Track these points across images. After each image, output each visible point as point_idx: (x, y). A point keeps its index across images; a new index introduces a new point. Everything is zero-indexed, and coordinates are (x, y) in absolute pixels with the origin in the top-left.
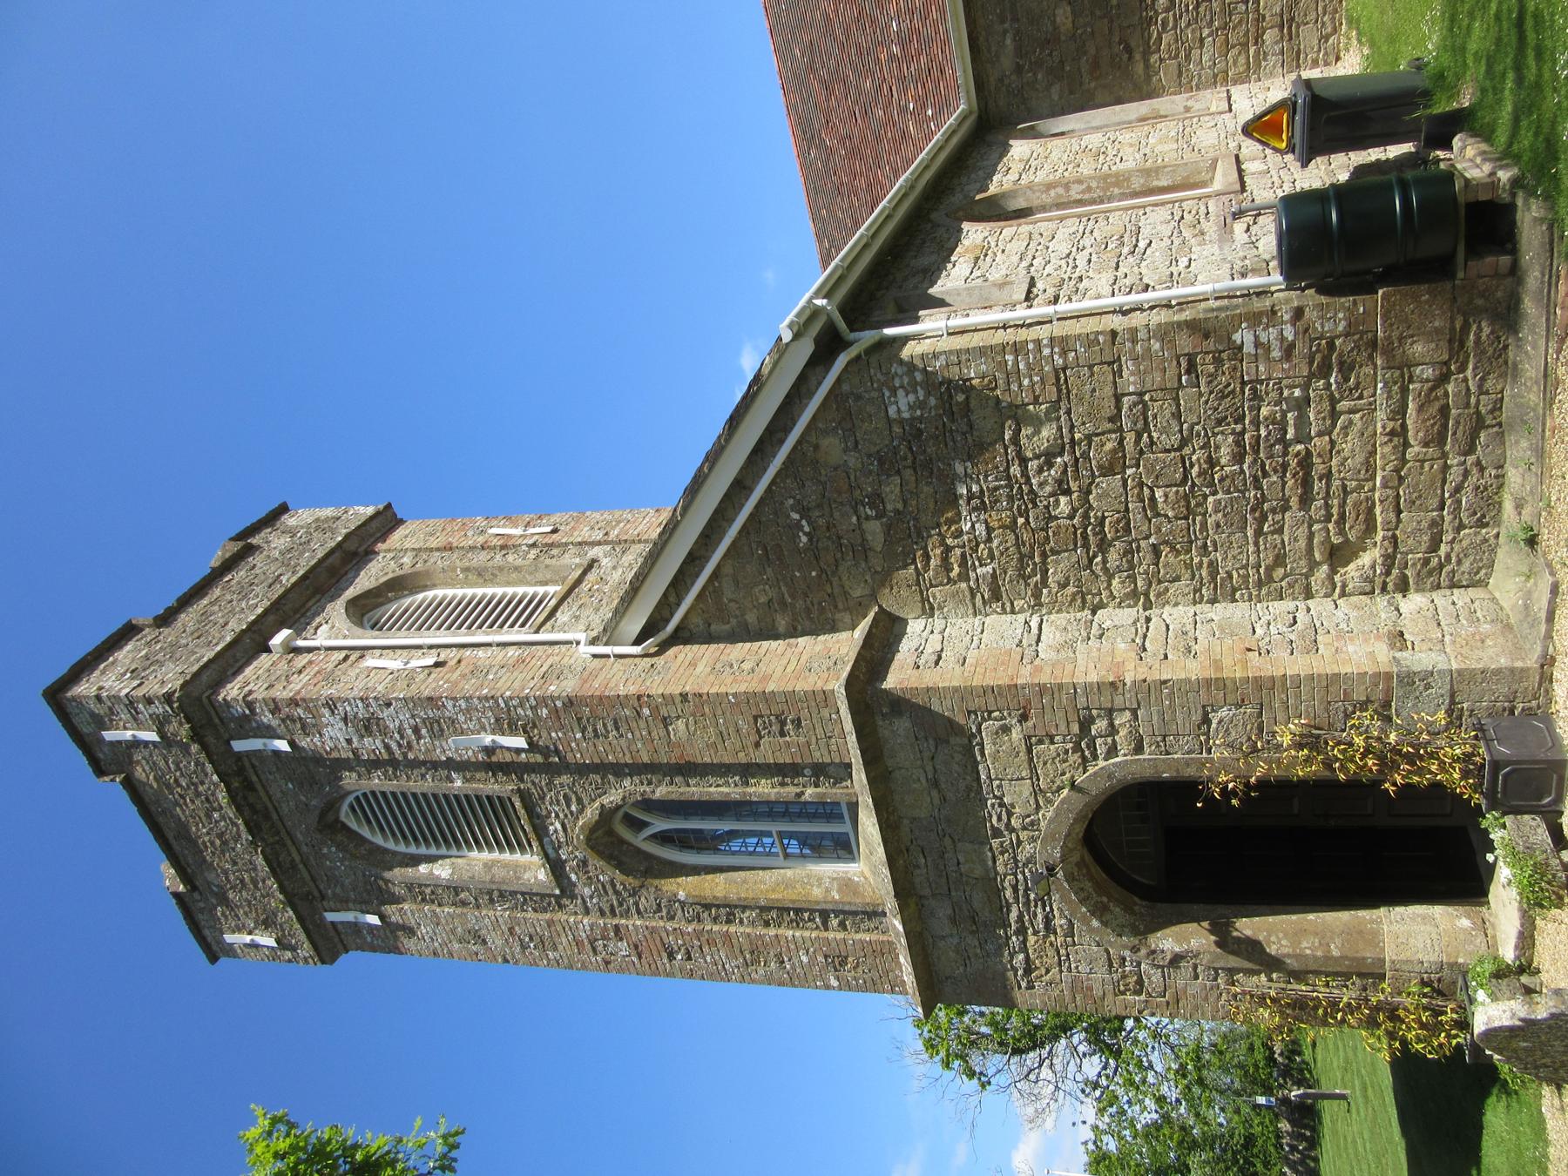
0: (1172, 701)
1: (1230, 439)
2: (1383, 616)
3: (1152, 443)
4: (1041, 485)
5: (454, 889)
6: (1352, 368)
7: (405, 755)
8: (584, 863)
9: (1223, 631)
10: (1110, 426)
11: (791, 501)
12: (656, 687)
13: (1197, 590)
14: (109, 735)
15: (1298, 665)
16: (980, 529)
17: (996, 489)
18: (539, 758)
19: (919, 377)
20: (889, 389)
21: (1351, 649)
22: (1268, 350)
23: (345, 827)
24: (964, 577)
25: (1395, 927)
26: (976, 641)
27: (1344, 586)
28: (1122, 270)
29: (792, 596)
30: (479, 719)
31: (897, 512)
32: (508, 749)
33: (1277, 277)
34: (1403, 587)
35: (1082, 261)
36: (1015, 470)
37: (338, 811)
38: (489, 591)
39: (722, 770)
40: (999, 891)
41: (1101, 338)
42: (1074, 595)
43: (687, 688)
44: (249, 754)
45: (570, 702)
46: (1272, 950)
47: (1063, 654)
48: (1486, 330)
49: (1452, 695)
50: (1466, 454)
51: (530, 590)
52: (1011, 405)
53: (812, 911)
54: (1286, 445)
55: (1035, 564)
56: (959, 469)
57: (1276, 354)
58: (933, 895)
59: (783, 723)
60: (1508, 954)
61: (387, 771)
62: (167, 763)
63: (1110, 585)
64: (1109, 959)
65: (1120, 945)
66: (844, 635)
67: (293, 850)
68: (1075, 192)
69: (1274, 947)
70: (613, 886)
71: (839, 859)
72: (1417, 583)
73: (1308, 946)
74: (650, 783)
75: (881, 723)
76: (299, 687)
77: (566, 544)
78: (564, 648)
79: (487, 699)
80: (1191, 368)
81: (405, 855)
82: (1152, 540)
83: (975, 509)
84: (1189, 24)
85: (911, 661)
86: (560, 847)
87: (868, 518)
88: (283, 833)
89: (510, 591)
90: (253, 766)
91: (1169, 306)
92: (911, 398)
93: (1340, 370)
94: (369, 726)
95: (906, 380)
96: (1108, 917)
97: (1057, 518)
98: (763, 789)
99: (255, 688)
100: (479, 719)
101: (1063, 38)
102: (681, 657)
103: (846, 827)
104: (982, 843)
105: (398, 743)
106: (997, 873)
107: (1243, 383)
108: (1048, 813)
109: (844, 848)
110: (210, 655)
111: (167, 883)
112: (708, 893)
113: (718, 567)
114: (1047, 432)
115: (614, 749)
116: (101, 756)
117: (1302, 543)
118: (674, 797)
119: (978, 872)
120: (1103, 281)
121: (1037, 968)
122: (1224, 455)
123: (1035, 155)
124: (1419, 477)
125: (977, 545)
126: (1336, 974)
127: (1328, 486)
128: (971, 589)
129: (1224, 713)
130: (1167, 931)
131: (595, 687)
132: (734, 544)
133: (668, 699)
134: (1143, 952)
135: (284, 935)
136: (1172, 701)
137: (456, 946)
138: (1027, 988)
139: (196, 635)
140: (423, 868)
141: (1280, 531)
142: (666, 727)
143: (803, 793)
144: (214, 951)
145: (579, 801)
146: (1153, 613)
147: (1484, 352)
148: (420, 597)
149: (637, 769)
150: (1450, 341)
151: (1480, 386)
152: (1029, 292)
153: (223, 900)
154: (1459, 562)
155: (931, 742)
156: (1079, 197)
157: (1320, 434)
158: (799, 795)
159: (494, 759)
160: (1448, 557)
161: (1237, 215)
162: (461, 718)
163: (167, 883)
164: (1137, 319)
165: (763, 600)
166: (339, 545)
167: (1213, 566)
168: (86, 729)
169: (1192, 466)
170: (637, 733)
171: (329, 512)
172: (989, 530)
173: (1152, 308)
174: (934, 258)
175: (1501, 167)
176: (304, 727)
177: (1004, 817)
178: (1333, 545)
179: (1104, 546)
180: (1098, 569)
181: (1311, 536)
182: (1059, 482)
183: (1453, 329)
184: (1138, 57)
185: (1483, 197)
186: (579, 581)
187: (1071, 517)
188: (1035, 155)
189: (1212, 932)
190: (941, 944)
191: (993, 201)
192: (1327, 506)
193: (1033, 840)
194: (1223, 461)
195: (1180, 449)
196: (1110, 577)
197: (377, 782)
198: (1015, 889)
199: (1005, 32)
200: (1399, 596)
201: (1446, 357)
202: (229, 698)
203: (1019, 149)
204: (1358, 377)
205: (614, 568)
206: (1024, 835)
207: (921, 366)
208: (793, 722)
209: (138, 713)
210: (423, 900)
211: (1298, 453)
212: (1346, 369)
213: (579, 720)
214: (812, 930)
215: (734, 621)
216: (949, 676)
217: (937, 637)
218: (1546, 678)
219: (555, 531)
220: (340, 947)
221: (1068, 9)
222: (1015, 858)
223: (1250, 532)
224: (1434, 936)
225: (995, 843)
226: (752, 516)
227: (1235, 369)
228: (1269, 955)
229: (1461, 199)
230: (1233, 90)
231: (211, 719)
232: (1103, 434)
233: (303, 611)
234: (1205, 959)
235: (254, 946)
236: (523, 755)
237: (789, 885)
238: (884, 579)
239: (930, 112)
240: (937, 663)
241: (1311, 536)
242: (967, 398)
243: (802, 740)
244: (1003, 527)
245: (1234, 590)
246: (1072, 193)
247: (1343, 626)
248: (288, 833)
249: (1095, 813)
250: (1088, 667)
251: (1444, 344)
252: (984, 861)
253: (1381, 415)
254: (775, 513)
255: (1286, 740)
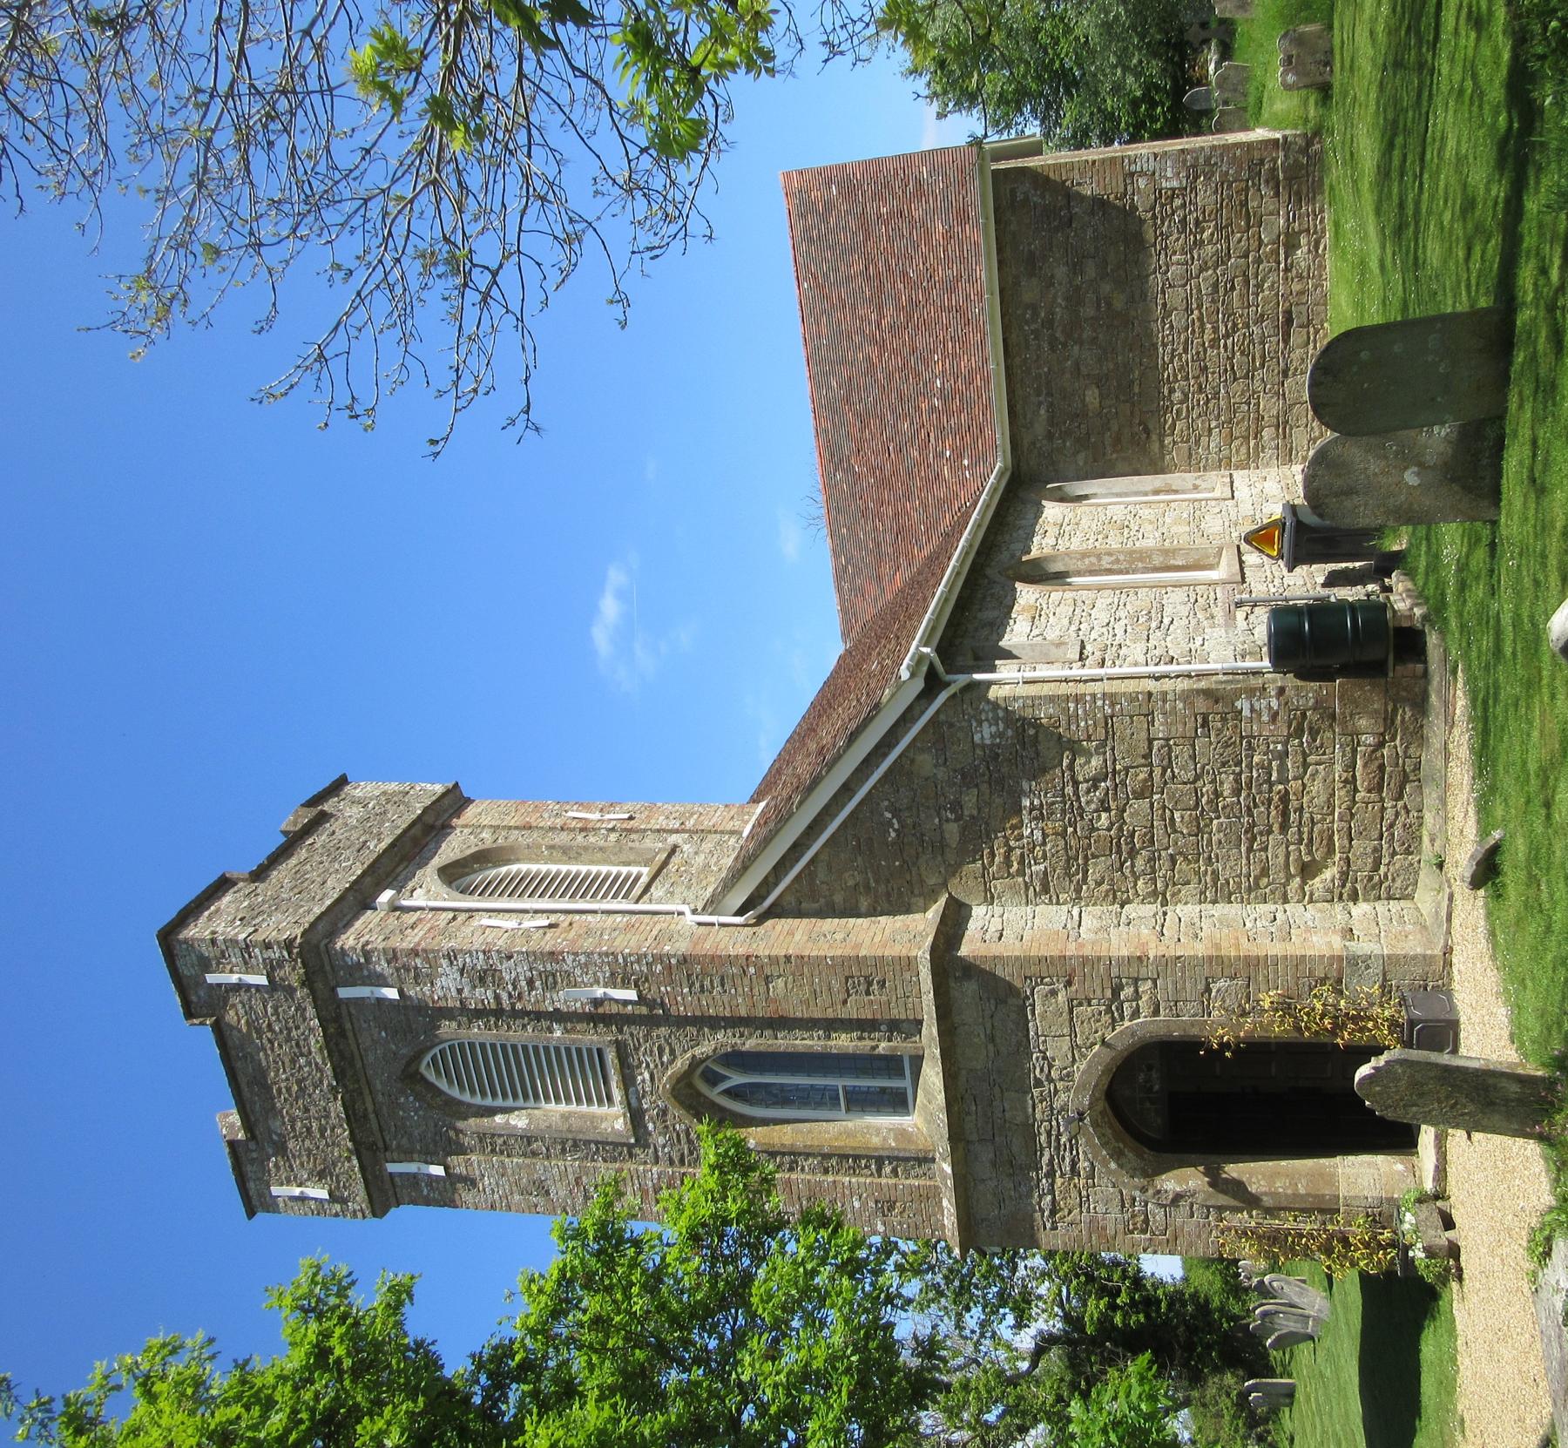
0: (1183, 973)
1: (1231, 777)
2: (1339, 917)
3: (1174, 776)
4: (1088, 803)
5: (528, 1138)
6: (1318, 732)
7: (513, 1005)
8: (664, 1112)
9: (1221, 923)
10: (1143, 761)
11: (886, 803)
12: (762, 949)
13: (1203, 893)
14: (211, 978)
15: (1276, 949)
16: (1038, 835)
17: (1053, 803)
18: (644, 1010)
19: (1001, 714)
20: (976, 720)
21: (1315, 939)
22: (1260, 715)
23: (423, 1079)
24: (1021, 872)
25: (1348, 1170)
26: (1029, 924)
27: (1312, 895)
28: (1152, 643)
29: (877, 882)
30: (595, 974)
31: (972, 817)
32: (617, 1001)
33: (1266, 663)
34: (1354, 897)
35: (1119, 631)
36: (1069, 790)
37: (420, 1063)
38: (574, 868)
39: (809, 1024)
40: (1034, 1137)
41: (1140, 697)
42: (1107, 891)
43: (791, 952)
44: (359, 1002)
45: (684, 960)
46: (1253, 1189)
47: (1100, 935)
48: (1409, 714)
49: (1384, 975)
50: (1397, 800)
51: (614, 870)
52: (1069, 740)
53: (869, 1158)
54: (1271, 785)
55: (1078, 865)
56: (1025, 786)
57: (1265, 718)
58: (980, 1140)
59: (870, 984)
60: (1429, 1186)
61: (489, 1021)
62: (265, 1007)
63: (1136, 885)
64: (1122, 1201)
65: (1131, 1186)
66: (918, 916)
67: (368, 1100)
68: (1106, 562)
69: (1254, 1187)
70: (688, 1134)
71: (895, 1113)
72: (1364, 895)
73: (1280, 1186)
74: (742, 1035)
75: (953, 985)
76: (417, 939)
77: (645, 830)
78: (668, 917)
79: (607, 955)
80: (1205, 723)
81: (480, 1107)
82: (1170, 851)
83: (1035, 819)
84: (1200, 415)
85: (978, 936)
86: (643, 1097)
87: (948, 820)
88: (363, 1081)
89: (594, 869)
90: (350, 1014)
91: (1189, 676)
92: (994, 729)
93: (1310, 733)
94: (484, 977)
95: (990, 715)
96: (1124, 1160)
97: (1098, 829)
98: (844, 1042)
99: (373, 939)
100: (595, 974)
101: (1091, 414)
102: (779, 928)
103: (906, 1083)
104: (1027, 1093)
105: (510, 994)
106: (1035, 1120)
107: (1242, 738)
108: (1082, 1065)
109: (899, 1102)
110: (318, 910)
111: (224, 1132)
112: (776, 1141)
113: (817, 854)
114: (1096, 762)
115: (715, 1006)
116: (194, 998)
117: (1281, 859)
118: (762, 1049)
119: (1019, 1120)
120: (1136, 651)
121: (1061, 1209)
122: (1227, 789)
123: (1067, 520)
124: (1365, 815)
125: (1034, 848)
126: (1302, 1210)
127: (1301, 817)
128: (1026, 883)
129: (1221, 984)
130: (1170, 1174)
131: (707, 947)
132: (833, 835)
133: (773, 960)
134: (1151, 1192)
135: (338, 1187)
136: (1183, 973)
137: (517, 1197)
138: (1052, 1229)
139: (296, 890)
140: (499, 1119)
141: (1265, 849)
142: (767, 984)
143: (877, 1046)
144: (254, 1202)
145: (672, 1052)
146: (1169, 909)
147: (1407, 728)
148: (504, 869)
149: (734, 1022)
150: (1385, 719)
151: (1405, 752)
152: (1081, 653)
153: (281, 1149)
154: (1394, 880)
155: (992, 1001)
156: (1109, 566)
157: (1295, 779)
158: (874, 1048)
159: (601, 1010)
160: (1386, 875)
161: (1239, 604)
162: (578, 972)
163: (224, 1132)
164: (1167, 685)
165: (851, 883)
166: (420, 817)
167: (1215, 874)
168: (186, 971)
169: (1202, 796)
170: (740, 989)
171: (393, 786)
172: (1045, 836)
173: (1177, 677)
174: (996, 613)
175: (1417, 605)
176: (416, 977)
177: (1046, 1069)
178: (1304, 863)
179: (1133, 853)
180: (1127, 872)
181: (1288, 854)
182: (1102, 802)
183: (1386, 711)
184: (1154, 437)
185: (1405, 624)
186: (665, 863)
187: (1109, 829)
188: (1067, 520)
189: (1206, 1174)
190: (981, 1187)
191: (1036, 562)
192: (1300, 833)
193: (1068, 1089)
194: (1225, 794)
195: (1194, 782)
196: (1137, 879)
197: (477, 1032)
198: (1049, 1134)
199: (1040, 403)
200: (1351, 904)
201: (1382, 730)
202: (346, 947)
203: (1052, 511)
204: (1322, 739)
205: (696, 853)
206: (1060, 1085)
207: (1003, 705)
208: (878, 982)
209: (250, 957)
210: (493, 1151)
211: (1280, 791)
212: (1314, 733)
213: (689, 976)
214: (867, 1176)
215: (822, 901)
216: (1010, 947)
217: (997, 920)
218: (1448, 964)
219: (631, 818)
220: (393, 1200)
221: (1096, 391)
222: (1051, 1106)
223: (1243, 849)
224: (1376, 1177)
225: (1036, 1092)
226: (852, 813)
227: (1236, 726)
228: (1250, 1193)
229: (1391, 625)
230: (1236, 474)
231: (323, 966)
232: (1137, 767)
233: (394, 875)
234: (1200, 1198)
235: (303, 1199)
236: (630, 1007)
237: (849, 1134)
238: (954, 870)
239: (966, 462)
240: (1000, 939)
241: (1288, 854)
242: (1037, 733)
243: (884, 998)
244: (1056, 834)
245: (1230, 894)
246: (1103, 562)
247: (1310, 923)
248: (368, 1083)
249: (1118, 1068)
250: (1120, 945)
251: (1381, 721)
252: (1025, 1109)
253: (1338, 768)
254: (872, 812)
255: (1267, 1005)
